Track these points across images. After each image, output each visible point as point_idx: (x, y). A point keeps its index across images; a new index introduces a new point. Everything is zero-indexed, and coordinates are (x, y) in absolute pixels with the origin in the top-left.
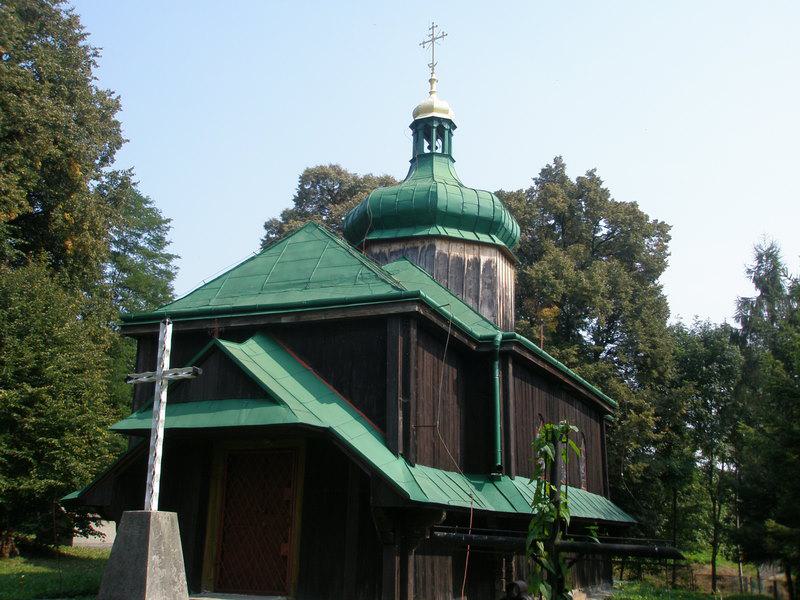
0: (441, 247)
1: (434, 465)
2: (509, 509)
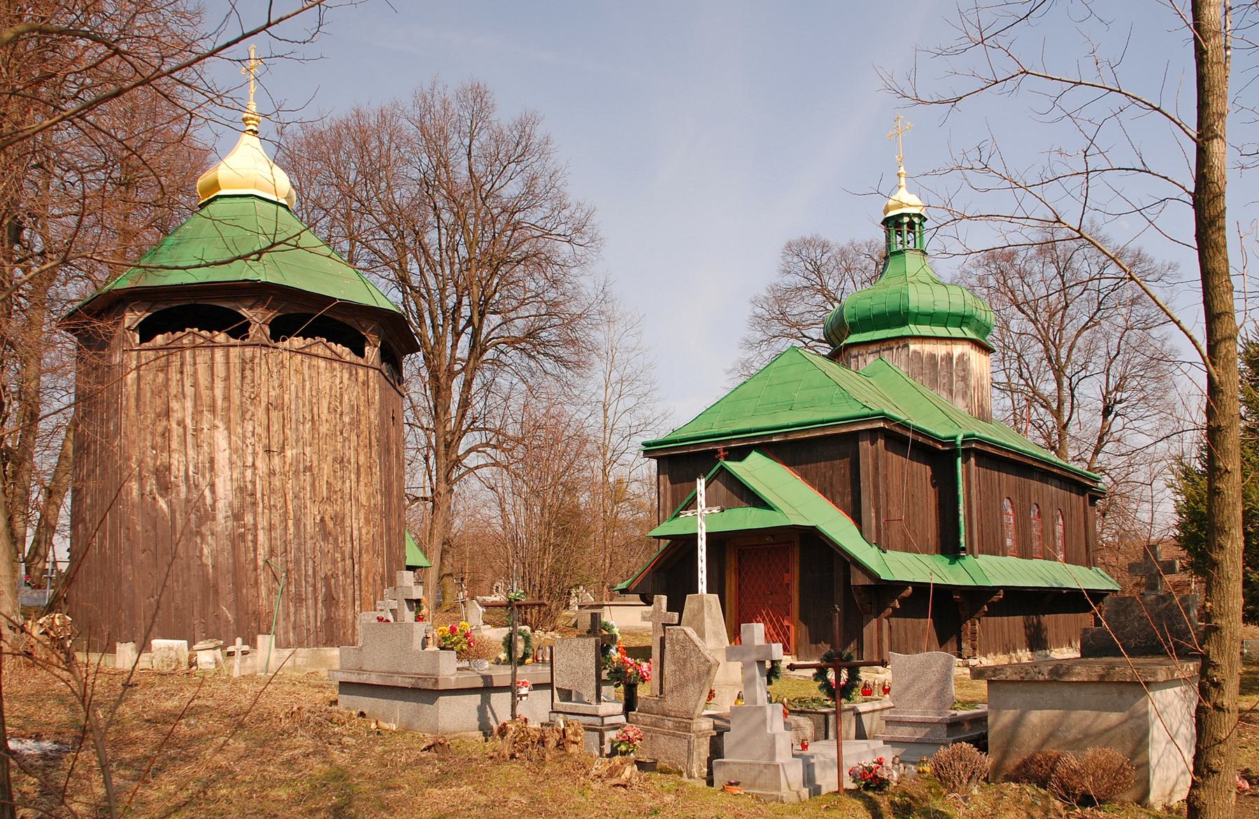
0: (914, 346)
1: (907, 548)
2: (973, 584)
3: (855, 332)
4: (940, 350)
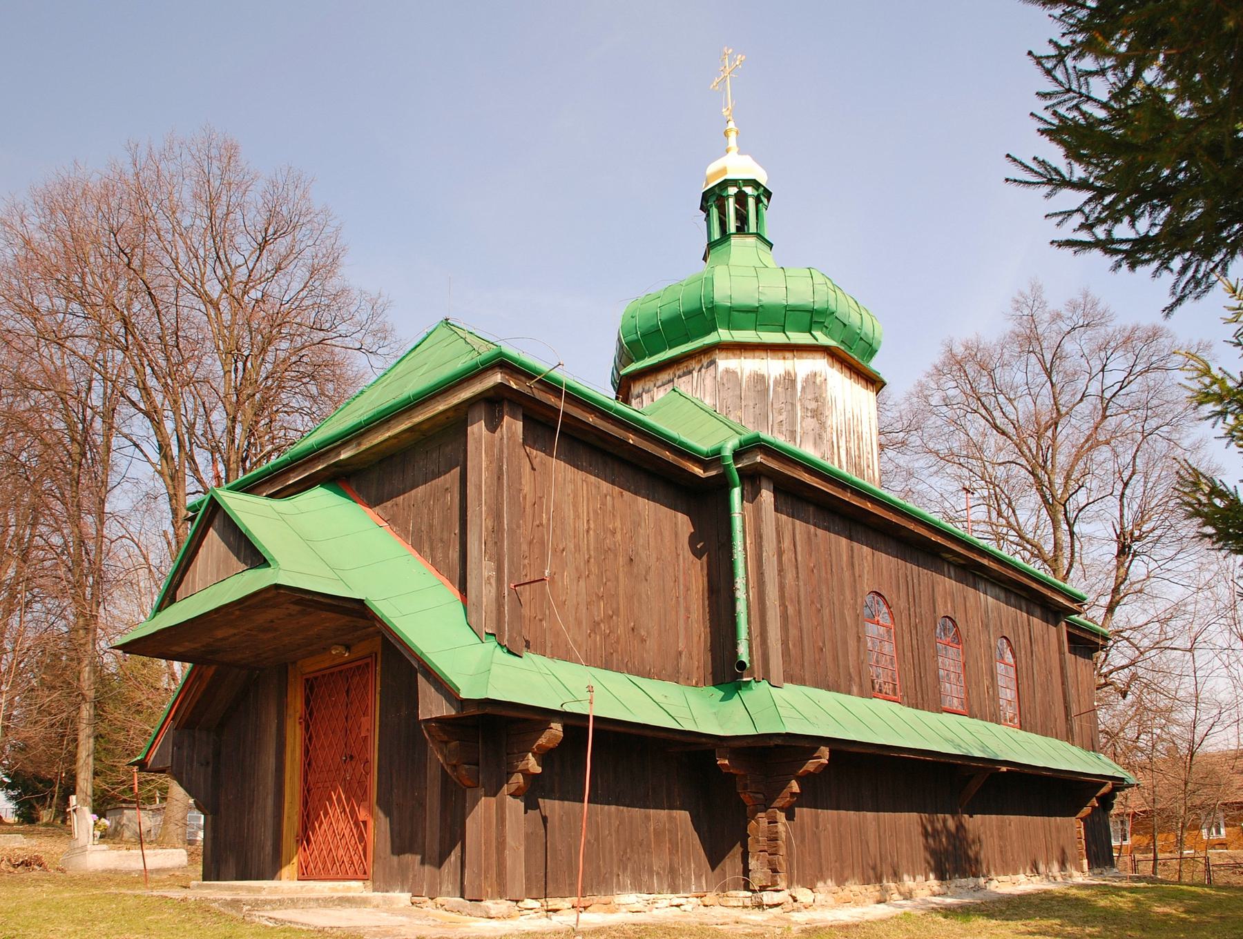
0: (725, 363)
2: (753, 732)
4: (773, 367)
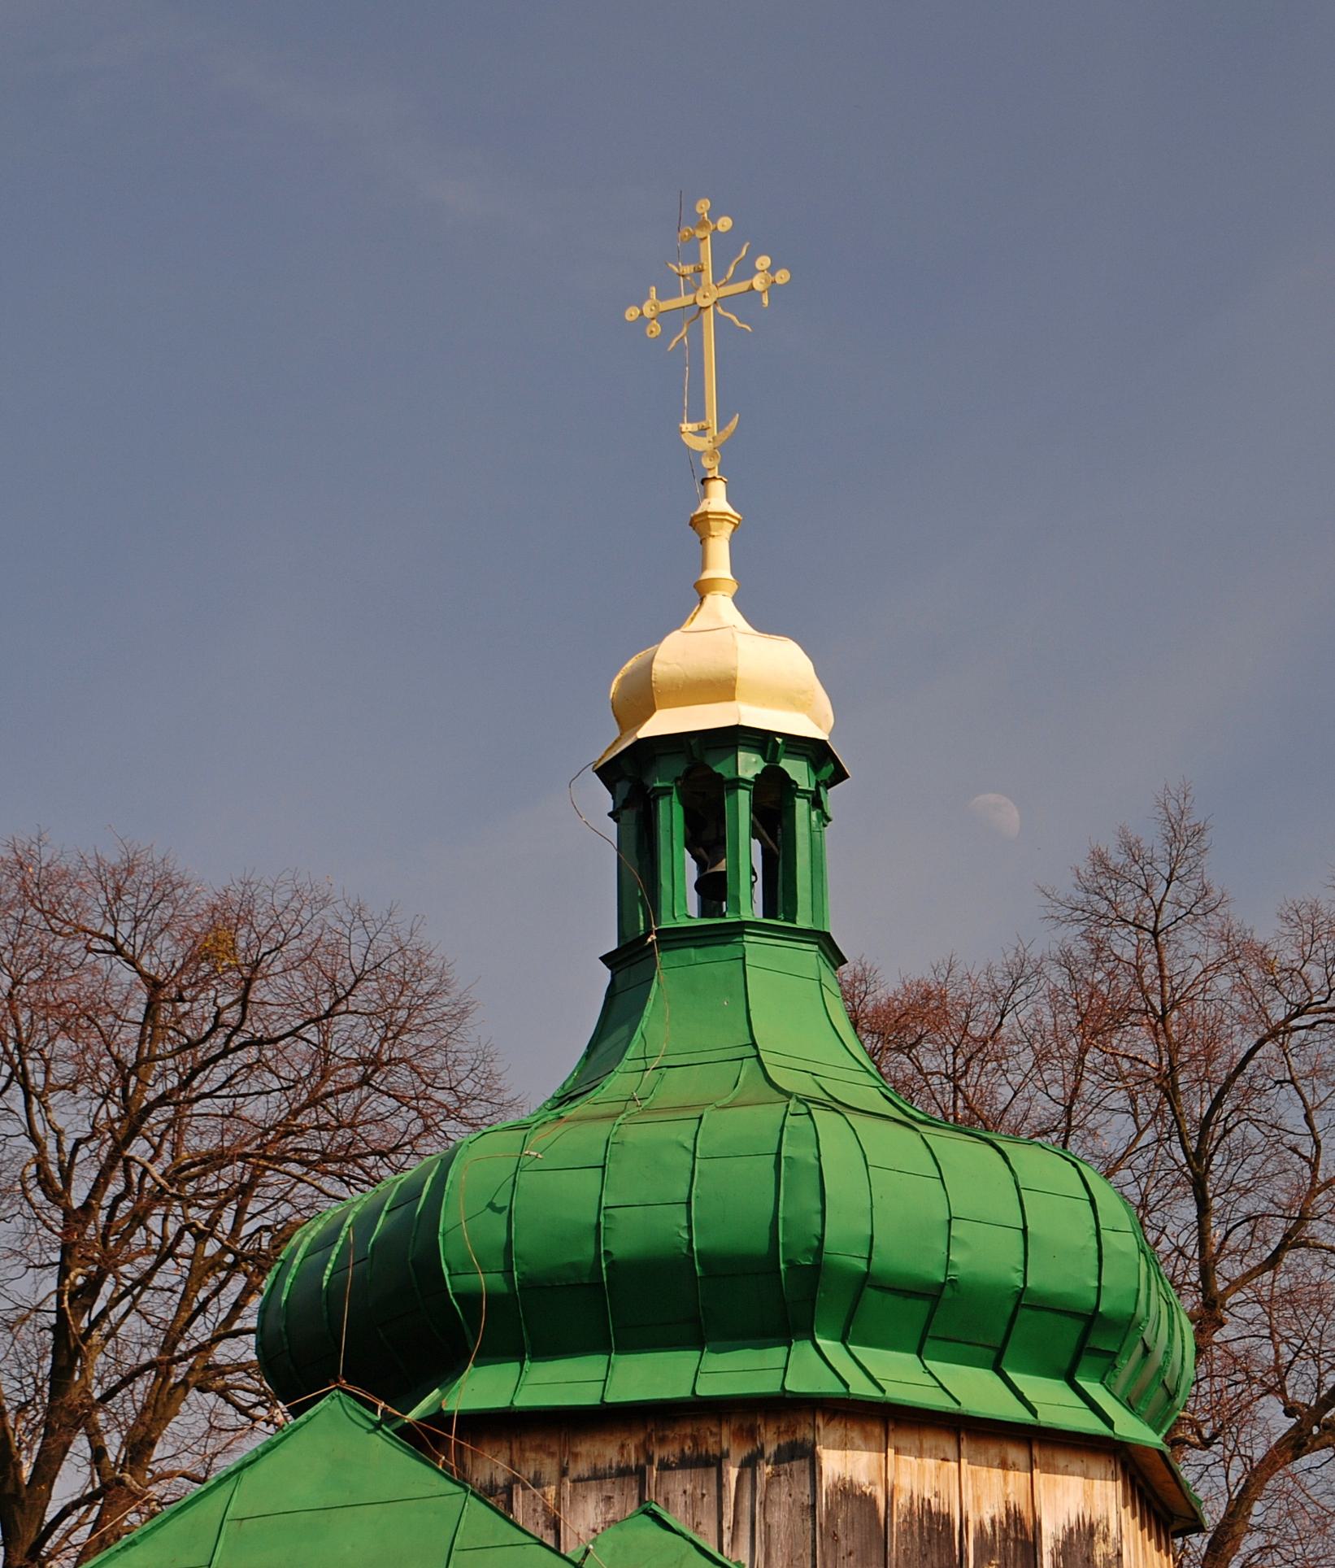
0: (844, 1462)
3: (493, 1354)
4: (980, 1492)
